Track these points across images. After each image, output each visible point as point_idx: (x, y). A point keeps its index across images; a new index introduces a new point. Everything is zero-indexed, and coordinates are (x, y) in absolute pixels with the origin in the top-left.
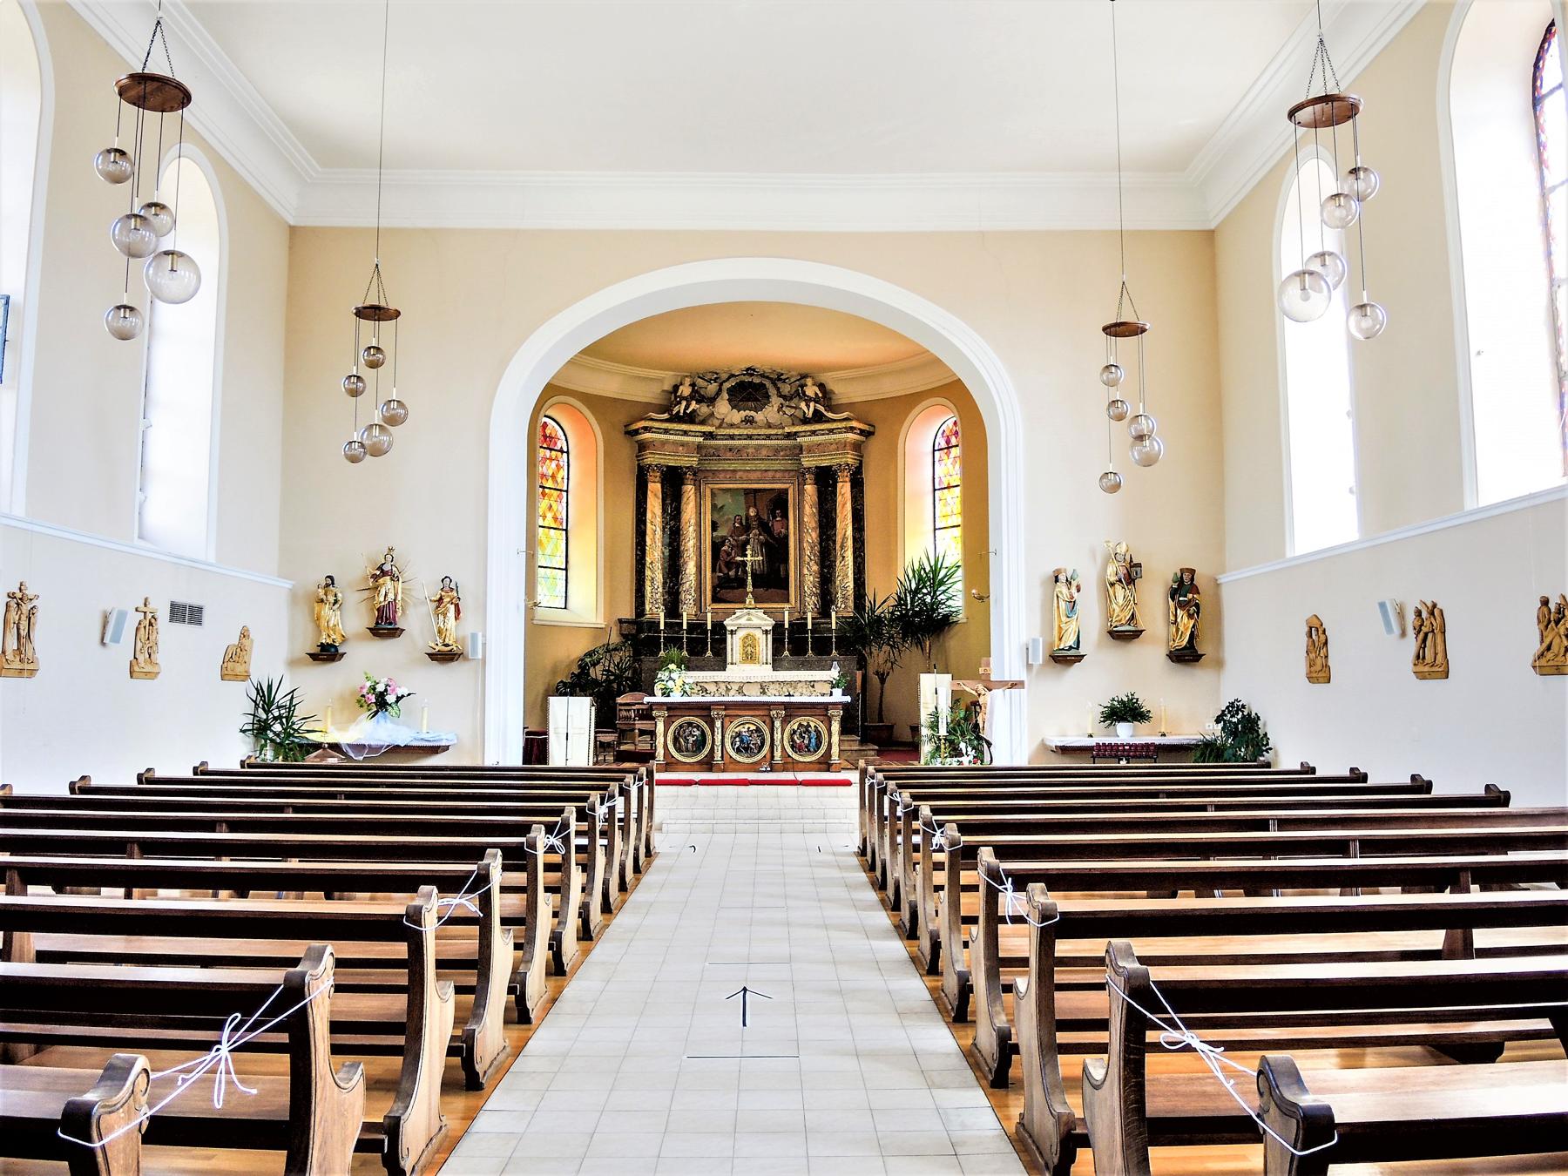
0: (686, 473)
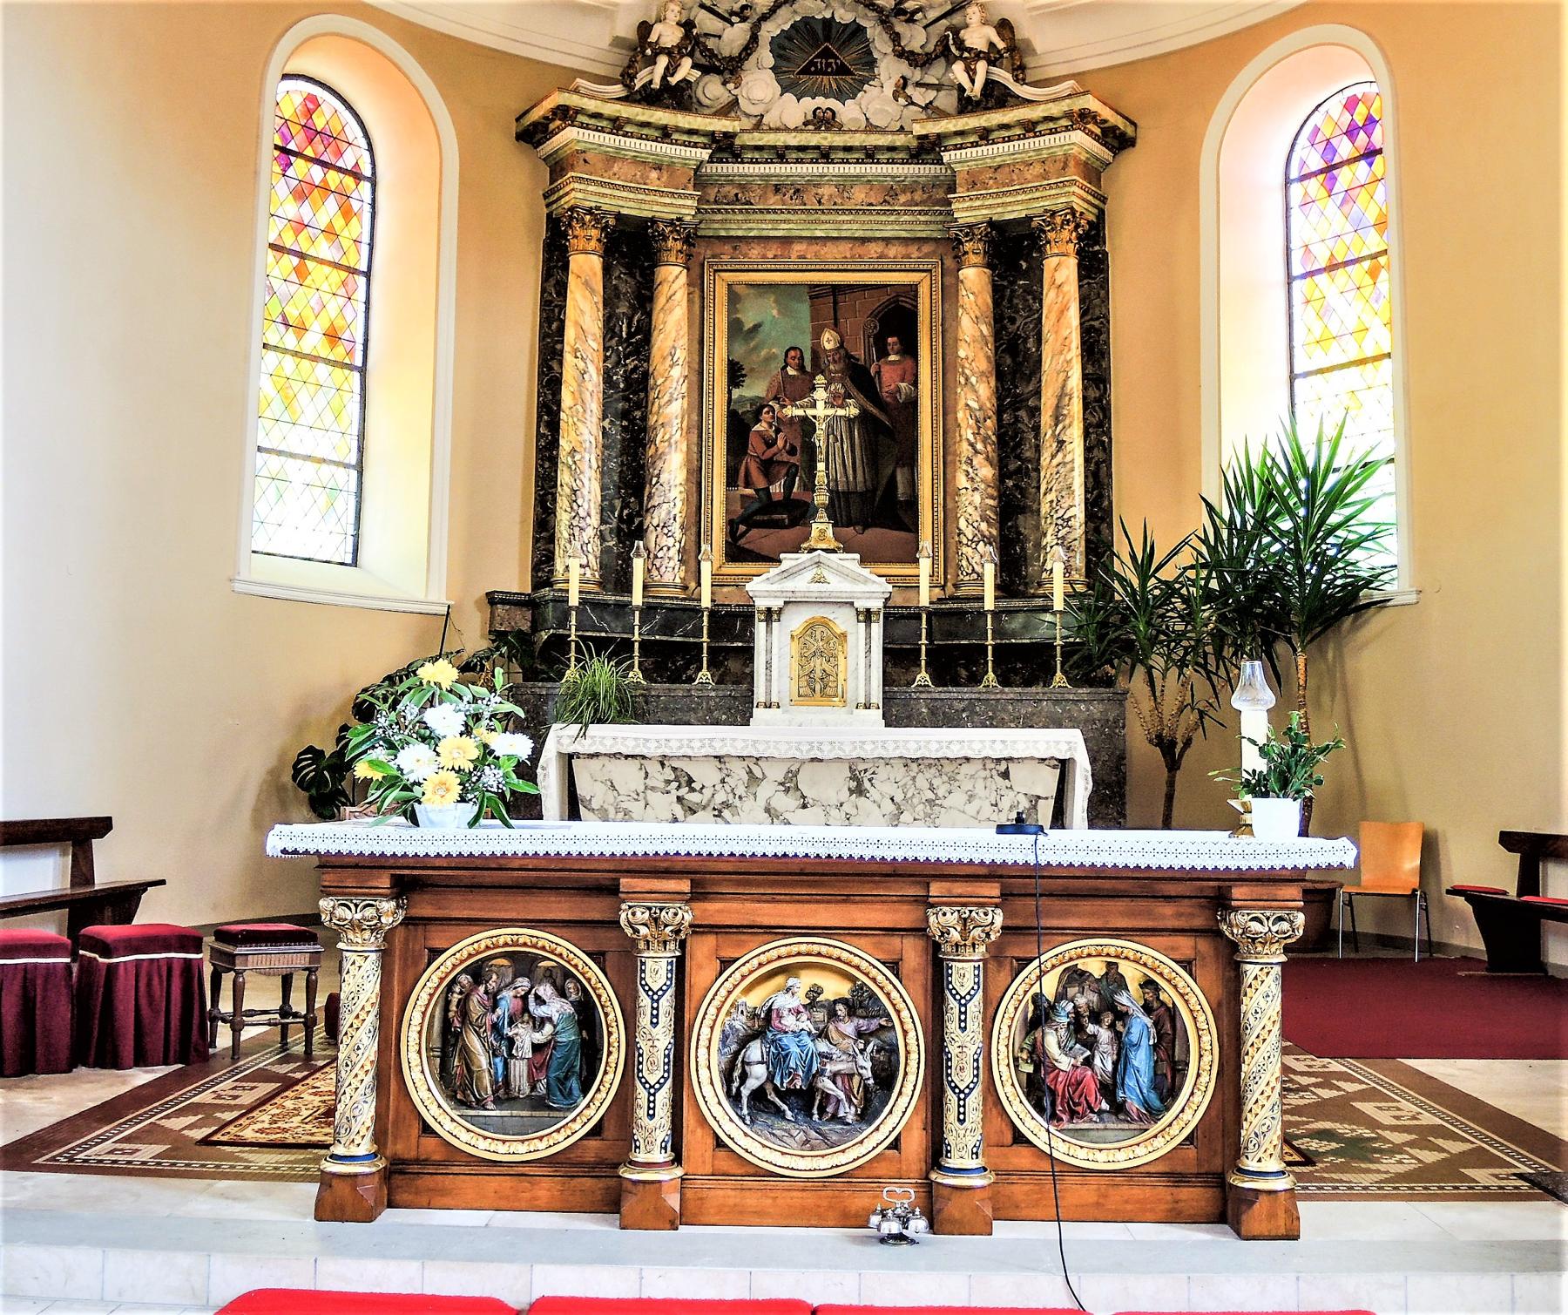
0: (665, 239)
